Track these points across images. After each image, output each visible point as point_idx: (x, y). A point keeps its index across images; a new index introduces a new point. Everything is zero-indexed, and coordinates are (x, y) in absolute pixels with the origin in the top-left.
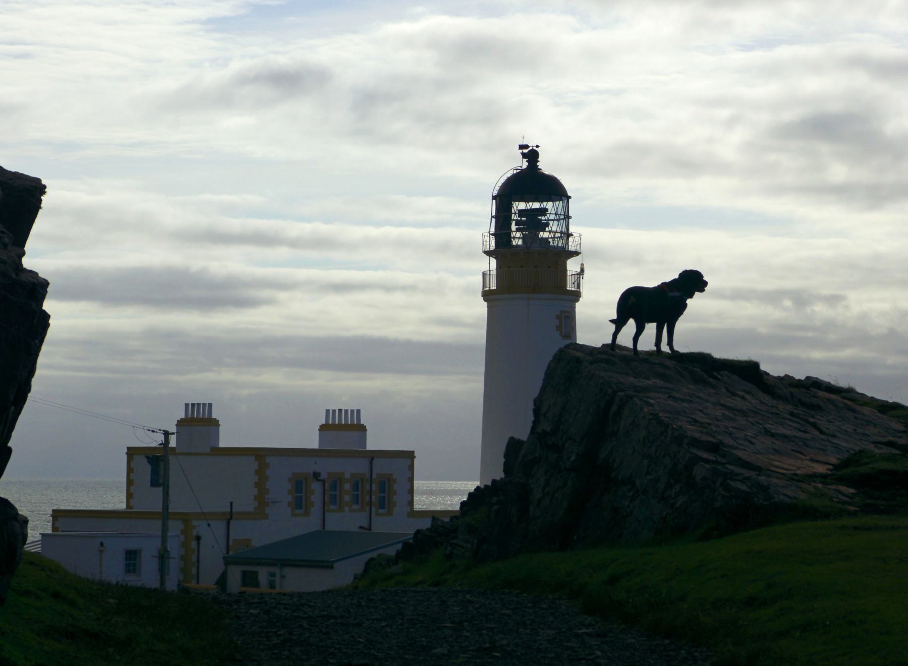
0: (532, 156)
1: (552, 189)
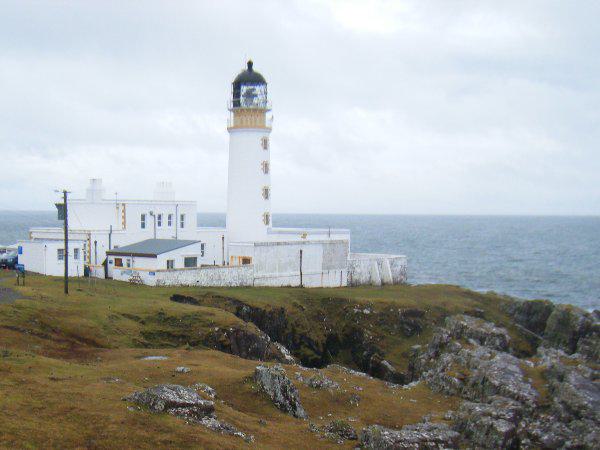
0: (250, 64)
1: (258, 80)
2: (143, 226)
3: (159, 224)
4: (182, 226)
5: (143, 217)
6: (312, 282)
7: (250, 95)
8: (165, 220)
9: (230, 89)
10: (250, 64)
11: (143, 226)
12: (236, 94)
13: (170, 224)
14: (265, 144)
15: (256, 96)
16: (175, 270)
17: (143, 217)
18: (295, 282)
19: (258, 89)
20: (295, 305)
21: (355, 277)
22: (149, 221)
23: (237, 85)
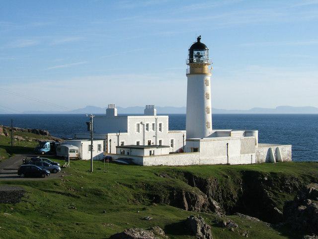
0: (199, 39)
5: (138, 125)
6: (232, 162)
8: (150, 127)
9: (188, 53)
10: (199, 39)
12: (191, 55)
15: (202, 56)
16: (156, 156)
18: (225, 162)
19: (201, 53)
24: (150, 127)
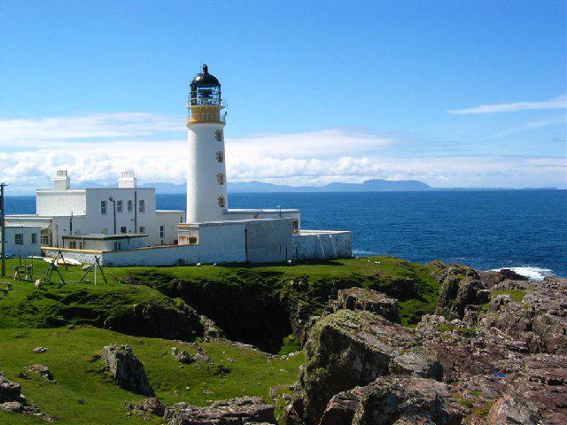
2: (104, 211)
3: (119, 209)
4: (141, 210)
7: (206, 95)
8: (125, 206)
10: (206, 69)
11: (104, 211)
12: (194, 95)
13: (129, 209)
14: (219, 136)
17: (103, 204)
20: (234, 280)
21: (300, 252)
22: (110, 206)
23: (194, 85)
24: (125, 206)
